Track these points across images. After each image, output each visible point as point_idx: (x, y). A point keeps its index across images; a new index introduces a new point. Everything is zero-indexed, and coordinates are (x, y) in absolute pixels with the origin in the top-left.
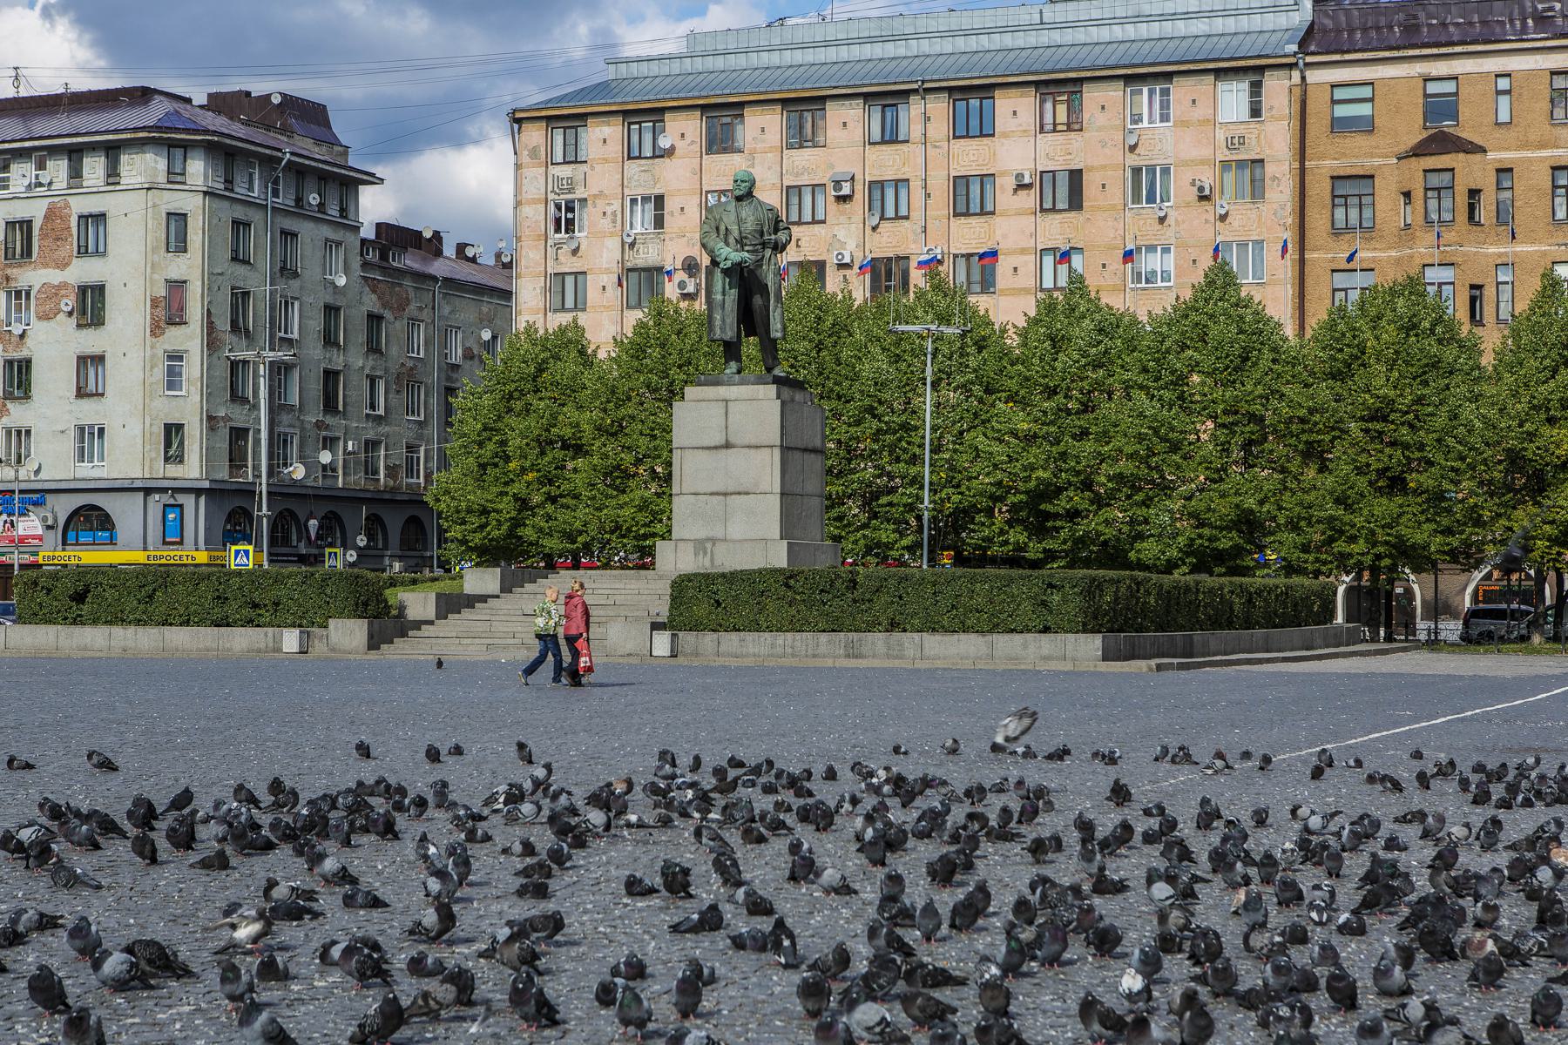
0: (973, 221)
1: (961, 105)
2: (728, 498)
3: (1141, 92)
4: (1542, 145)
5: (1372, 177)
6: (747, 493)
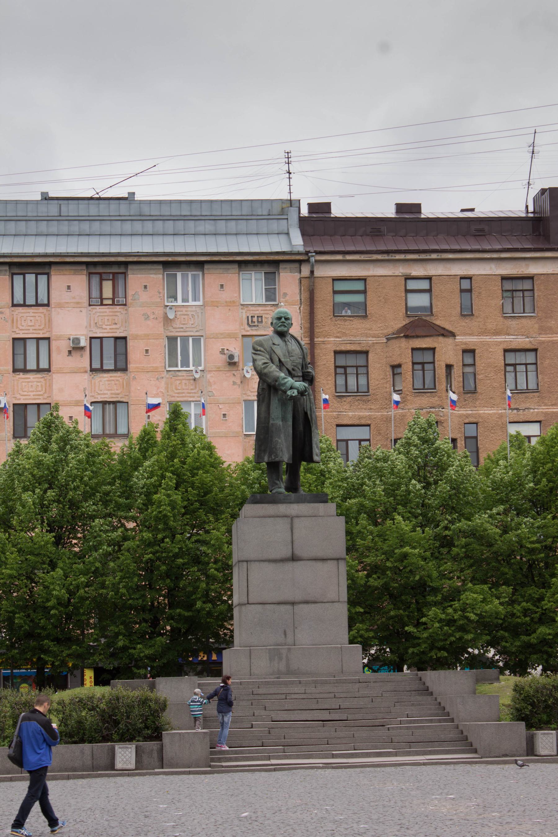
0: (31, 376)
1: (18, 280)
2: (296, 607)
3: (187, 275)
4: (497, 333)
5: (366, 353)
6: (315, 602)
